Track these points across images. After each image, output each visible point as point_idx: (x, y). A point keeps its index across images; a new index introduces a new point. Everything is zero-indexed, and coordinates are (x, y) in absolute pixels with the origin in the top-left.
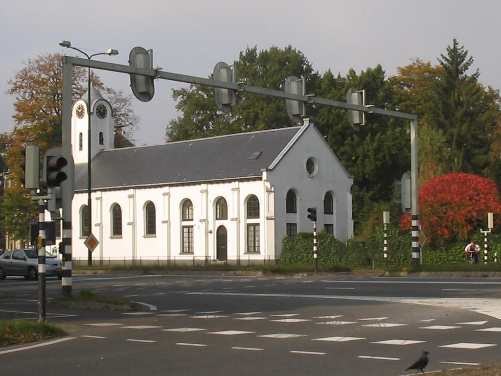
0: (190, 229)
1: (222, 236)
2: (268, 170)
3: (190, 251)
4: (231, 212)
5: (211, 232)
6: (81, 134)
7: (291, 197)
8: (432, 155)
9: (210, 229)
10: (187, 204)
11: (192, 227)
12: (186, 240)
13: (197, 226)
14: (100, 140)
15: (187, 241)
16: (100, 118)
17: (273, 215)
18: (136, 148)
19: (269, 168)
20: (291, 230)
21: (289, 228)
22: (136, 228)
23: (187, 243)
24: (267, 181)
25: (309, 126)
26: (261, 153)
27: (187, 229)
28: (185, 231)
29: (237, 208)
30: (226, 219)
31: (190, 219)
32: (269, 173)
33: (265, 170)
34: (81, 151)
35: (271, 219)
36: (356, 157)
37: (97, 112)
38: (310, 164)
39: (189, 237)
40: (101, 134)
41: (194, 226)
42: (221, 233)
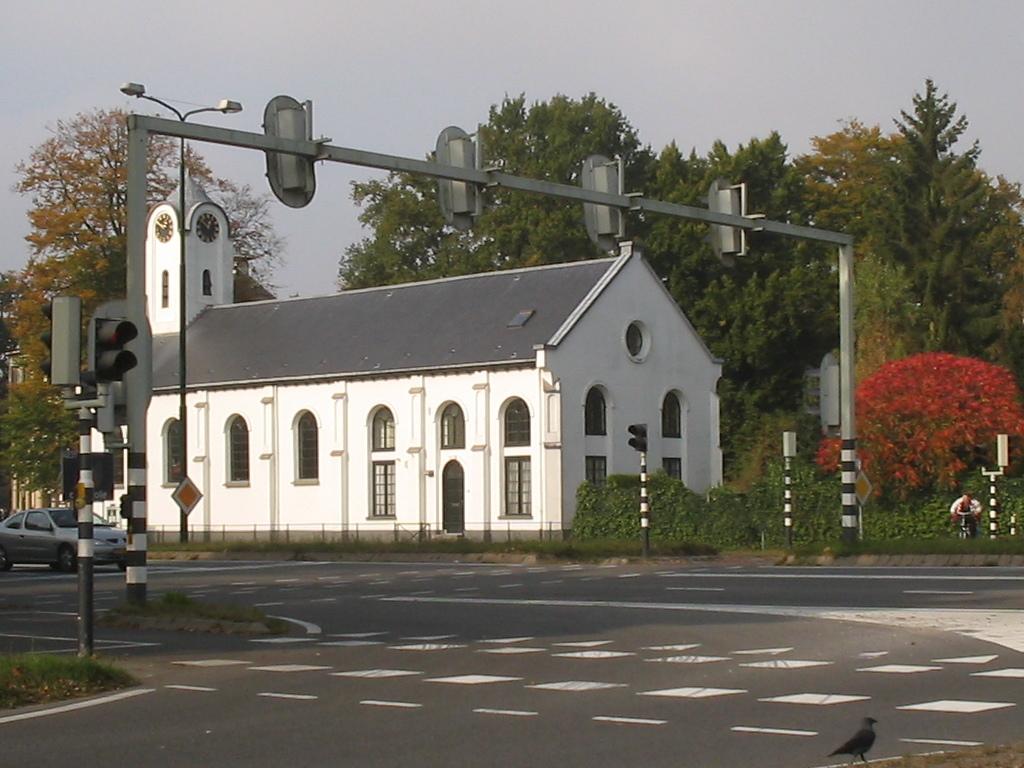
0: (389, 467)
1: (453, 481)
2: (547, 348)
3: (389, 513)
4: (473, 434)
5: (431, 474)
6: (166, 274)
7: (595, 403)
9: (428, 468)
10: (381, 417)
11: (392, 463)
12: (380, 490)
14: (204, 287)
15: (383, 492)
17: (559, 440)
18: (278, 303)
19: (550, 343)
21: (591, 466)
22: (279, 466)
23: (383, 497)
24: (545, 369)
25: (631, 257)
26: (534, 312)
27: (383, 467)
29: (483, 424)
31: (388, 446)
32: (550, 353)
33: (542, 346)
34: (166, 309)
35: (555, 447)
36: (727, 322)
37: (198, 230)
38: (634, 335)
39: (386, 485)
40: (206, 273)
41: (397, 462)
42: (451, 475)
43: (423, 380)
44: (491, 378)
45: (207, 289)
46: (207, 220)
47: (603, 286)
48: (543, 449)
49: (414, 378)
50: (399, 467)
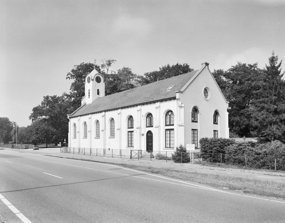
0: (132, 133)
1: (149, 137)
3: (132, 146)
4: (155, 122)
5: (143, 135)
8: (29, 135)
9: (142, 133)
10: (131, 118)
11: (133, 131)
12: (130, 142)
13: (135, 131)
14: (98, 93)
15: (130, 143)
16: (98, 82)
17: (183, 122)
18: (85, 64)
20: (194, 133)
23: (130, 141)
25: (205, 67)
27: (130, 133)
28: (129, 134)
29: (159, 119)
30: (152, 127)
34: (174, 129)
35: (182, 126)
36: (239, 81)
39: (131, 141)
40: (98, 90)
41: (134, 131)
42: (149, 135)
43: (91, 116)
44: (92, 116)
45: (98, 93)
46: (98, 78)
47: (197, 75)
48: (178, 126)
49: (156, 103)
50: (134, 133)
